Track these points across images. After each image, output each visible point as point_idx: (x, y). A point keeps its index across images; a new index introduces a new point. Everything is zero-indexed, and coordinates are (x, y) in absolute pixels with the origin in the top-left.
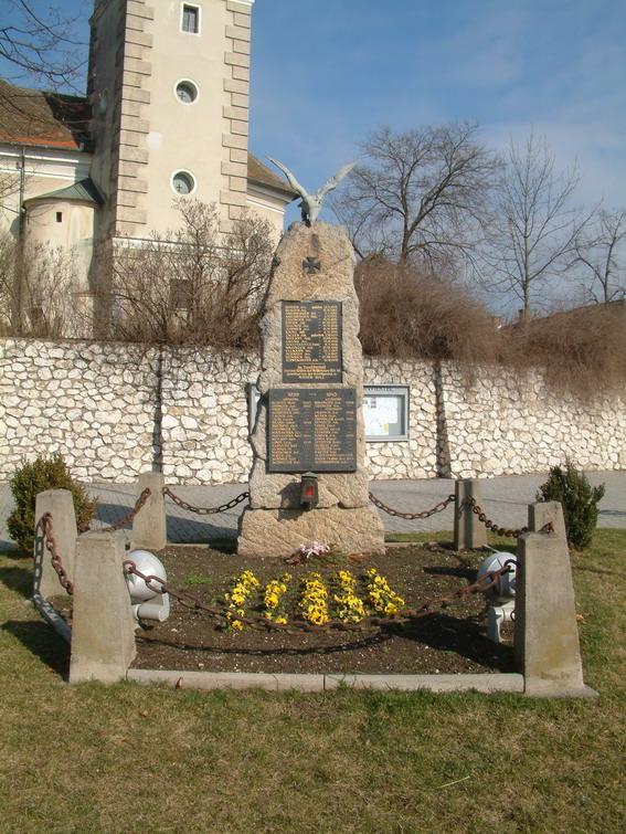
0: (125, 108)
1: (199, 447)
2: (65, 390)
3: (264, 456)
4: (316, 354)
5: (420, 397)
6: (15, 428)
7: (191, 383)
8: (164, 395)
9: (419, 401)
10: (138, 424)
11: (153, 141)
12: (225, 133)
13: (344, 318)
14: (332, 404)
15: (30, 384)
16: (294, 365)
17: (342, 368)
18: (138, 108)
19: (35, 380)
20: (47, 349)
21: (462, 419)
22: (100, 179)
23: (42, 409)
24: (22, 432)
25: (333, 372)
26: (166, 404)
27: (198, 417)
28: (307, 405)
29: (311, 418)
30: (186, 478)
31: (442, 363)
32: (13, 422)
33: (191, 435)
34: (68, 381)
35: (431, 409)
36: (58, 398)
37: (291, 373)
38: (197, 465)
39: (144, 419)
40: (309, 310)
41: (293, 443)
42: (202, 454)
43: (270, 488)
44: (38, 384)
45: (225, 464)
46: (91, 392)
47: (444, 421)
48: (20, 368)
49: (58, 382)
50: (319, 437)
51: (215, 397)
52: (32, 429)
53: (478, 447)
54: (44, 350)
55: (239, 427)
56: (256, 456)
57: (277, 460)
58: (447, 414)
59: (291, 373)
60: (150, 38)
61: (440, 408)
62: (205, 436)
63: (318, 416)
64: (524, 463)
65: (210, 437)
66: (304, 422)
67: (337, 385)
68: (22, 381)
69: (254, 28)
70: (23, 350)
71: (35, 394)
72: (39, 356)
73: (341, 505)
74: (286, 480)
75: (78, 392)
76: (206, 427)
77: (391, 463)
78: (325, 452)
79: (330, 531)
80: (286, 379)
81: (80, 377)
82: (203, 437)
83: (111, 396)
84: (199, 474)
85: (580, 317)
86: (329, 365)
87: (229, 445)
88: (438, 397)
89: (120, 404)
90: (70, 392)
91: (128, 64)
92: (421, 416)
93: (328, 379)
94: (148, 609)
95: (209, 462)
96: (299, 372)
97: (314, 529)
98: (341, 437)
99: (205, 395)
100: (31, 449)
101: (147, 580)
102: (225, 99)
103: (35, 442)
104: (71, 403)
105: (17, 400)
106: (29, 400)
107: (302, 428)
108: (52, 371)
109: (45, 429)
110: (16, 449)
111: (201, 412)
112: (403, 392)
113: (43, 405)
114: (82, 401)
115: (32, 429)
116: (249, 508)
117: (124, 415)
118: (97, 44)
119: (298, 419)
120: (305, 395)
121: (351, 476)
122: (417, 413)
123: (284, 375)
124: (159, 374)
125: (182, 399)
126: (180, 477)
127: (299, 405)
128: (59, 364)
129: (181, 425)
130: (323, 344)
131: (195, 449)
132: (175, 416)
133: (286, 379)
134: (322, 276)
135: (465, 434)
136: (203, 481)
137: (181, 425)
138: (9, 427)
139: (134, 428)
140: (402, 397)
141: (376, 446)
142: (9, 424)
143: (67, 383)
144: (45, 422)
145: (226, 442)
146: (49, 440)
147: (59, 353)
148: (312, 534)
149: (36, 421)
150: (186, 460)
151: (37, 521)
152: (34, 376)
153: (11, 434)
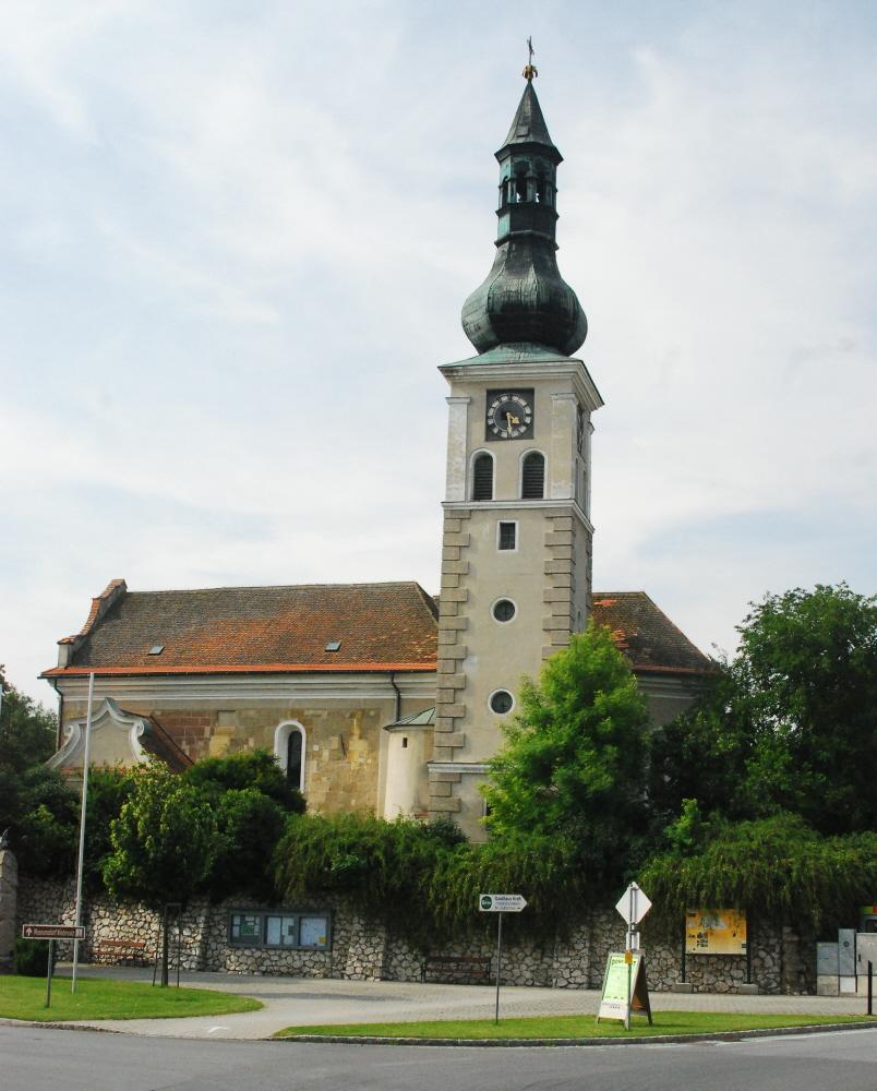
135: (364, 947)
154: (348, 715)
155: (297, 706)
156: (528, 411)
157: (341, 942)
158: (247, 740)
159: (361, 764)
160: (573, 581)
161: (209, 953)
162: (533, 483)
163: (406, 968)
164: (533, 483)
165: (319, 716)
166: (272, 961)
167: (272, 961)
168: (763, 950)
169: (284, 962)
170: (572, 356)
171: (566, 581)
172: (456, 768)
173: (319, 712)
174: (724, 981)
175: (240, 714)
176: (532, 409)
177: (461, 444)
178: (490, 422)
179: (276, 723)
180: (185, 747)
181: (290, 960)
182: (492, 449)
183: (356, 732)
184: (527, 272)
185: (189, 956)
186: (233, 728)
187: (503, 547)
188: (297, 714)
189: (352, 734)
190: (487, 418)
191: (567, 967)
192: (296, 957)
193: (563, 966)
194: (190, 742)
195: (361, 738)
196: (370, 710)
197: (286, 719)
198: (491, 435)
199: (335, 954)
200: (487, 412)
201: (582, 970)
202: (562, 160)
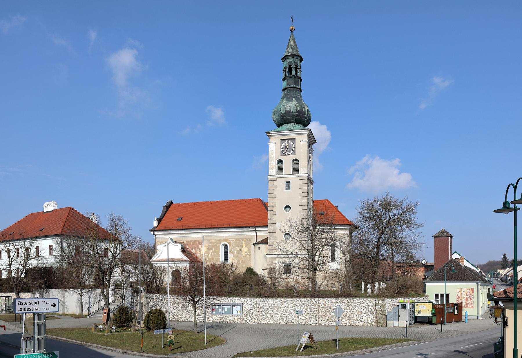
42: (200, 317)
53: (255, 317)
55: (210, 312)
60: (276, 186)
64: (271, 321)
85: (508, 286)
92: (245, 310)
102: (300, 208)
105: (178, 306)
135: (252, 314)
146: (182, 313)
154: (241, 240)
155: (226, 238)
156: (293, 146)
157: (245, 313)
158: (212, 248)
159: (246, 255)
160: (308, 199)
161: (206, 316)
162: (296, 170)
163: (264, 320)
164: (296, 170)
165: (233, 241)
166: (225, 319)
167: (225, 319)
168: (370, 313)
169: (228, 319)
170: (306, 127)
171: (306, 199)
172: (274, 256)
173: (233, 240)
174: (358, 322)
175: (209, 241)
176: (295, 145)
177: (273, 157)
178: (282, 150)
179: (221, 243)
180: (193, 251)
181: (230, 318)
182: (283, 158)
183: (244, 245)
184: (292, 100)
185: (201, 318)
186: (208, 245)
187: (287, 189)
188: (226, 240)
189: (243, 246)
190: (281, 148)
191: (312, 319)
192: (232, 317)
193: (311, 318)
194: (195, 249)
195: (246, 247)
196: (248, 238)
197: (223, 242)
198: (283, 154)
199: (243, 316)
200: (281, 147)
201: (316, 319)
202: (303, 60)
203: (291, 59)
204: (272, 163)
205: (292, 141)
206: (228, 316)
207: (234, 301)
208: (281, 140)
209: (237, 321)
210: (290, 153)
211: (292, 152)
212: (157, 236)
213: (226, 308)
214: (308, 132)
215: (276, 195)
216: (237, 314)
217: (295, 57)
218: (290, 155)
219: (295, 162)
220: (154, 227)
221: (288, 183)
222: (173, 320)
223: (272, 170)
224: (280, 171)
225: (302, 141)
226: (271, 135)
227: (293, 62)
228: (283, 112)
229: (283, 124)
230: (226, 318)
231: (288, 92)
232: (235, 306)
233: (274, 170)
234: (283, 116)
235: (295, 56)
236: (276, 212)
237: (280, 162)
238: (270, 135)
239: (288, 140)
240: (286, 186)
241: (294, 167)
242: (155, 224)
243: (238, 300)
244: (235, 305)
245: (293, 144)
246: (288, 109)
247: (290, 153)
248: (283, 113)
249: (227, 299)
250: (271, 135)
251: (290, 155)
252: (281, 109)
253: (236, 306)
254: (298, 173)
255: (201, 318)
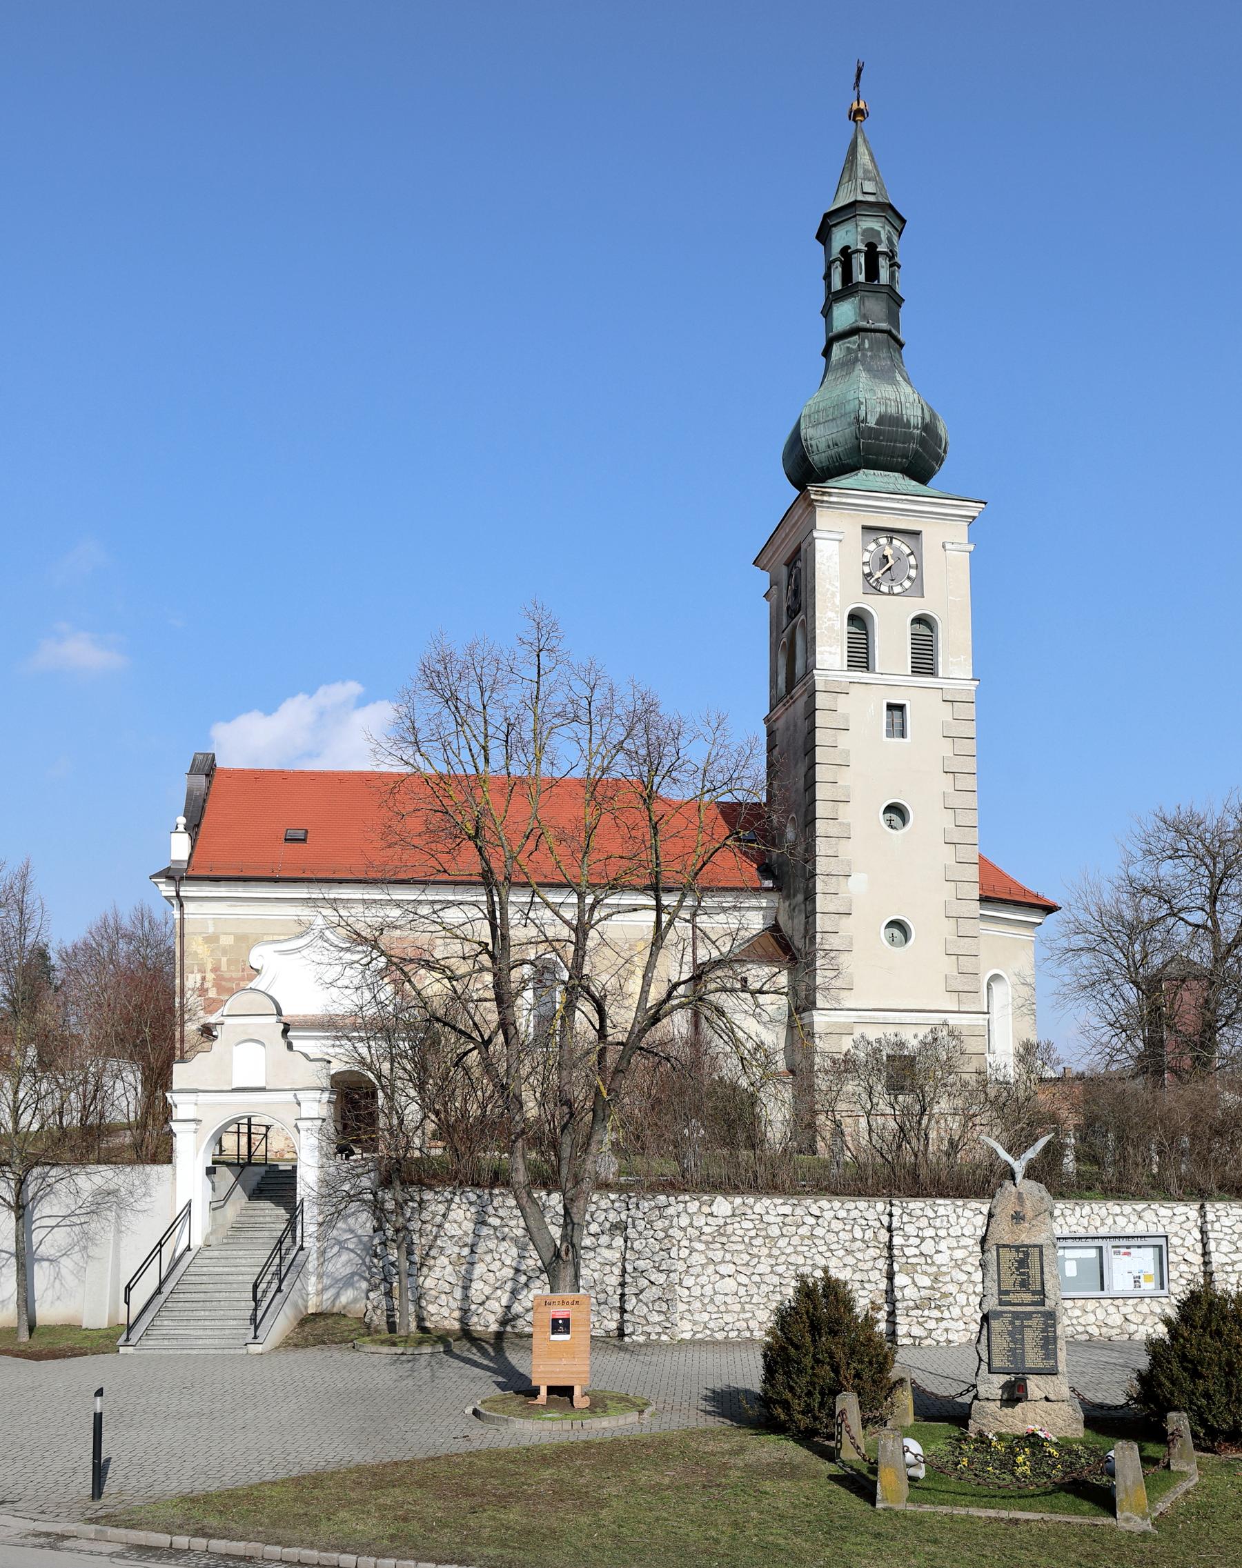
0: (821, 847)
1: (933, 1306)
2: (795, 1247)
3: (987, 1361)
4: (1024, 1284)
5: (1182, 1245)
6: (746, 1286)
7: (923, 1239)
8: (896, 1252)
9: (1180, 1250)
10: (869, 1281)
11: (857, 885)
12: (947, 863)
13: (1045, 1258)
14: (1036, 1323)
15: (756, 1242)
16: (1007, 1293)
17: (1044, 1295)
18: (836, 844)
19: (765, 1238)
20: (775, 1206)
21: (1234, 1271)
22: (792, 928)
23: (772, 1266)
24: (754, 1290)
25: (1037, 1298)
26: (898, 1262)
27: (931, 1274)
28: (1018, 1323)
29: (1022, 1333)
30: (921, 1338)
31: (1208, 1206)
32: (743, 1279)
33: (924, 1293)
34: (797, 1237)
35: (1198, 1259)
36: (788, 1255)
37: (1004, 1298)
38: (931, 1324)
39: (875, 1276)
40: (1018, 1252)
41: (1009, 1351)
42: (936, 1314)
43: (992, 1386)
44: (767, 1241)
45: (961, 1323)
46: (820, 1249)
47: (1211, 1274)
48: (749, 1225)
49: (788, 1239)
50: (1028, 1348)
51: (950, 1252)
52: (763, 1286)
54: (772, 1206)
56: (981, 1360)
57: (997, 1363)
58: (1214, 1267)
59: (1004, 1298)
60: (846, 718)
61: (1207, 1258)
62: (939, 1295)
63: (1027, 1332)
65: (945, 1295)
66: (1016, 1336)
67: (1040, 1308)
68: (751, 1238)
69: (978, 720)
70: (752, 1208)
71: (765, 1251)
72: (768, 1213)
73: (1047, 1399)
74: (1004, 1378)
75: (807, 1248)
76: (940, 1285)
77: (1149, 1321)
78: (1033, 1357)
79: (1038, 1418)
80: (1001, 1303)
81: (809, 1234)
82: (938, 1295)
83: (842, 1253)
84: (934, 1334)
86: (1034, 1293)
87: (964, 1303)
88: (1204, 1245)
89: (850, 1260)
90: (799, 1249)
91: (821, 792)
92: (1183, 1267)
93: (1033, 1304)
94: (912, 1472)
95: (945, 1322)
96: (1011, 1298)
97: (1026, 1416)
98: (1045, 1347)
99: (938, 1252)
100: (762, 1307)
101: (916, 1456)
102: (947, 819)
103: (766, 1299)
104: (801, 1260)
105: (745, 1256)
106: (759, 1257)
107: (1014, 1341)
108: (781, 1228)
109: (775, 1286)
110: (747, 1307)
111: (934, 1269)
112: (1162, 1242)
113: (773, 1263)
114: (812, 1258)
115: (763, 1286)
116: (976, 1397)
117: (854, 1272)
118: (776, 752)
119: (1011, 1334)
120: (1016, 1315)
121: (1054, 1378)
122: (1178, 1264)
123: (1000, 1299)
124: (889, 1229)
125: (916, 1256)
126: (914, 1337)
127: (1012, 1323)
128: (788, 1220)
129: (914, 1282)
130: (1029, 1277)
131: (930, 1308)
132: (908, 1274)
133: (1001, 1303)
134: (1027, 1225)
136: (938, 1342)
137: (914, 1282)
138: (739, 1284)
139: (866, 1285)
140: (1160, 1247)
141: (1130, 1302)
142: (740, 1281)
143: (796, 1240)
144: (776, 1280)
145: (962, 1299)
147: (787, 1210)
148: (1022, 1420)
149: (767, 1279)
150: (920, 1320)
151: (837, 1413)
152: (763, 1233)
153: (742, 1291)
162: (924, 662)
164: (924, 662)
166: (1070, 1318)
167: (1070, 1318)
177: (833, 595)
178: (867, 570)
182: (873, 605)
192: (1112, 1309)
203: (875, 219)
204: (829, 619)
205: (906, 539)
206: (1091, 1305)
207: (1109, 1221)
208: (864, 528)
209: (1142, 1329)
210: (897, 589)
211: (907, 584)
212: (189, 907)
213: (1067, 1263)
214: (976, 514)
215: (847, 752)
216: (1138, 1293)
217: (890, 215)
218: (898, 594)
219: (922, 629)
220: (174, 862)
221: (896, 708)
222: (719, 1336)
223: (827, 649)
224: (861, 656)
225: (948, 546)
226: (825, 498)
227: (882, 232)
228: (869, 417)
229: (858, 469)
230: (1078, 1313)
231: (867, 346)
232: (1123, 1250)
233: (839, 650)
234: (860, 429)
235: (890, 212)
236: (849, 825)
237: (858, 619)
238: (822, 502)
239: (891, 532)
240: (891, 724)
241: (930, 638)
242: (180, 847)
243: (1134, 1218)
244: (1127, 1241)
245: (912, 553)
246: (892, 410)
247: (897, 589)
248: (872, 422)
249: (1067, 1212)
250: (825, 498)
251: (898, 594)
252: (861, 403)
253: (1128, 1247)
254: (932, 672)
255: (942, 1319)
